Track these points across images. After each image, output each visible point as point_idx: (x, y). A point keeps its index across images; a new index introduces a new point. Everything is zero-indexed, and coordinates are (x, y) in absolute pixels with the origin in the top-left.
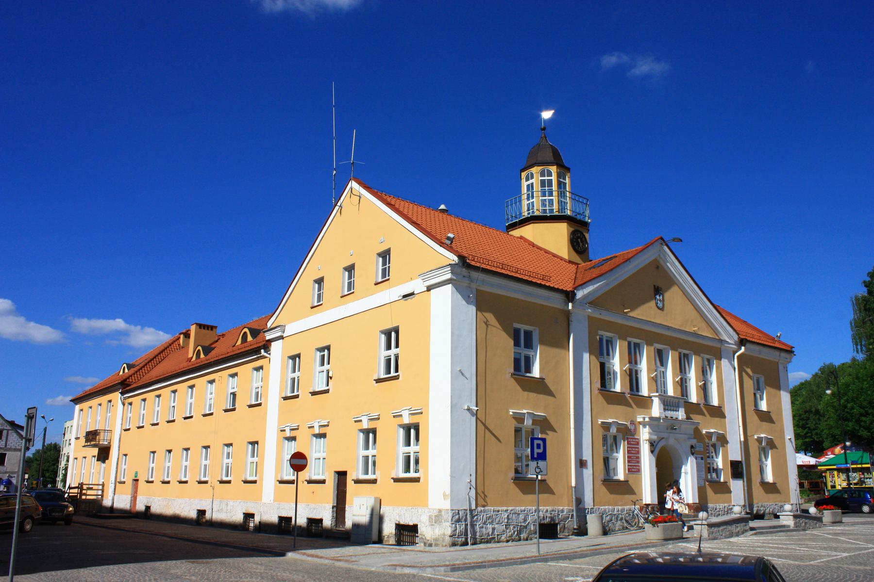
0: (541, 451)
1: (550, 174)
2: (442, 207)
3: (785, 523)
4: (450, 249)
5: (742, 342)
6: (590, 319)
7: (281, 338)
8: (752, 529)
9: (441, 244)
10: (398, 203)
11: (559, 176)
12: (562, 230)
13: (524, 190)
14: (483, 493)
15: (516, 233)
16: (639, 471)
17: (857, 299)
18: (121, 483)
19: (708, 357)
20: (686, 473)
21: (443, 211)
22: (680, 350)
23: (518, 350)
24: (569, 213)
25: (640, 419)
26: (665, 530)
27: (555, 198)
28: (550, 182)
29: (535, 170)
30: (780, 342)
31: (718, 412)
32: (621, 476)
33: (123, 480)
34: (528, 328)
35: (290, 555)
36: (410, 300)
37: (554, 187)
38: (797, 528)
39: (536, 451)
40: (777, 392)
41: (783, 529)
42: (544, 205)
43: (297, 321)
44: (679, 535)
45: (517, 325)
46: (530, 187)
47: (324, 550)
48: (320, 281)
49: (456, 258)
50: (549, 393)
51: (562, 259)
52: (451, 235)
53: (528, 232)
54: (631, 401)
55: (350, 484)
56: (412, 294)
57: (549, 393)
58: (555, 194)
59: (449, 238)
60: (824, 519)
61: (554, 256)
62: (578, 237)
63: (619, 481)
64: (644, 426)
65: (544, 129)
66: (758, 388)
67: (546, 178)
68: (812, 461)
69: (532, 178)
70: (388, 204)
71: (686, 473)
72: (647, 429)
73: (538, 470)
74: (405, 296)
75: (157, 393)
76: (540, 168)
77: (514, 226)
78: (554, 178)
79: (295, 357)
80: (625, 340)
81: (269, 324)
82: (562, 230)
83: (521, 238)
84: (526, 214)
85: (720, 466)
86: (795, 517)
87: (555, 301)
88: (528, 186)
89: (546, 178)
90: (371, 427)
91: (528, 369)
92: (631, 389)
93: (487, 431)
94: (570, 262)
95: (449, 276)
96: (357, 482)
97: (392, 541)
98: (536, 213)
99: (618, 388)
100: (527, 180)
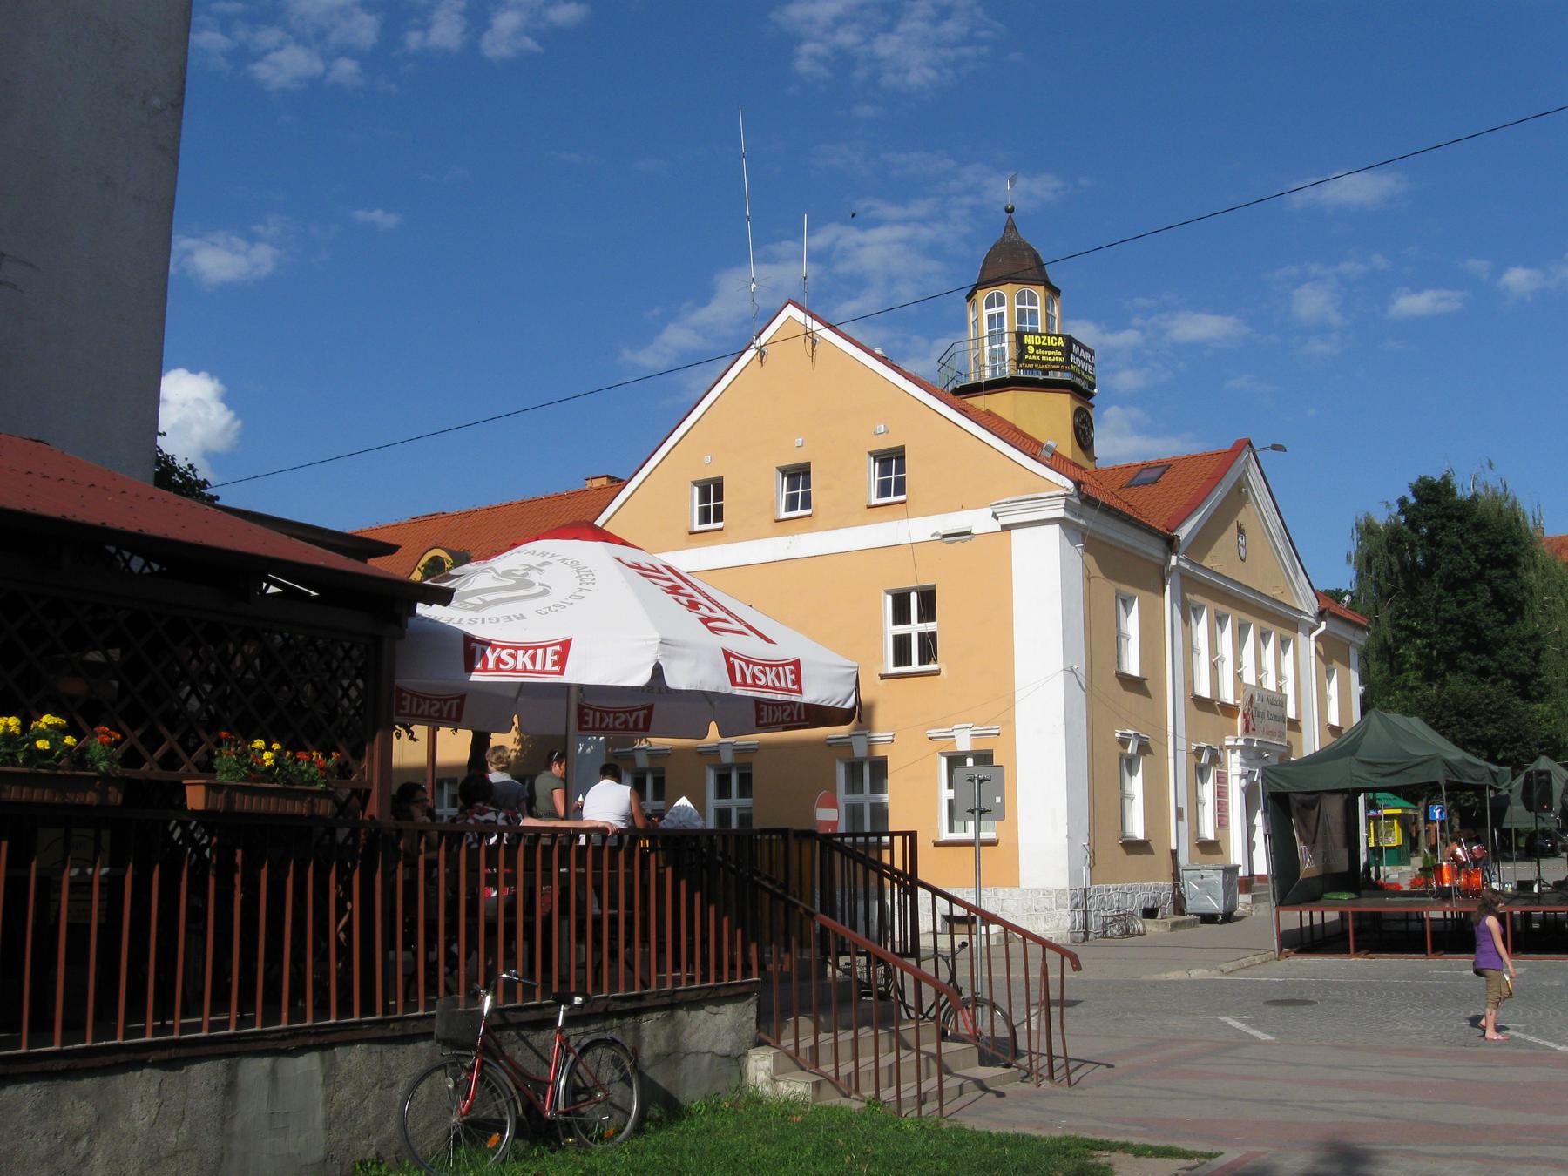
1: (1033, 301)
5: (1321, 615)
11: (1048, 305)
12: (1062, 405)
16: (1227, 824)
17: (1367, 530)
19: (739, 691)
25: (1227, 743)
29: (1007, 290)
36: (958, 546)
49: (1070, 485)
50: (1146, 693)
51: (1065, 459)
56: (969, 533)
57: (1146, 693)
64: (1233, 751)
69: (1001, 303)
74: (945, 536)
76: (1017, 288)
84: (988, 375)
87: (1154, 549)
100: (989, 305)
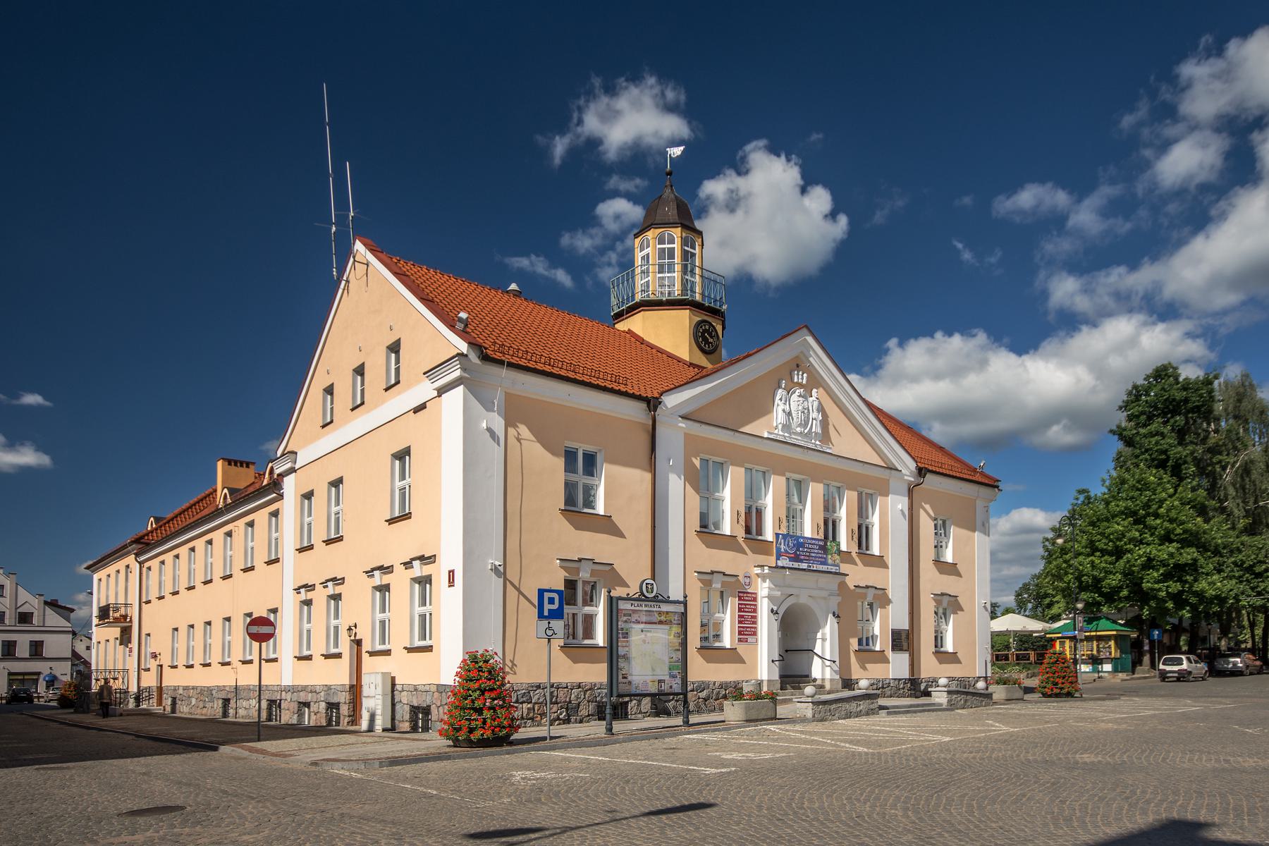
0: (555, 606)
2: (513, 286)
3: (937, 700)
4: (463, 334)
6: (687, 436)
7: (292, 470)
8: (882, 708)
9: (452, 327)
10: (407, 267)
11: (685, 242)
12: (683, 320)
13: (638, 262)
14: (512, 662)
15: (622, 326)
18: (267, 661)
20: (824, 640)
21: (517, 294)
22: (788, 475)
23: (573, 477)
24: (698, 297)
26: (747, 708)
27: (677, 275)
28: (672, 251)
29: (651, 234)
30: (982, 474)
31: (880, 562)
32: (727, 642)
33: (272, 656)
34: (590, 448)
35: (225, 749)
37: (677, 259)
38: (952, 706)
39: (547, 607)
40: (970, 533)
41: (936, 708)
42: (662, 286)
43: (311, 445)
44: (770, 714)
45: (572, 444)
46: (646, 258)
47: (274, 742)
48: (329, 390)
51: (679, 360)
52: (463, 315)
53: (637, 324)
54: (857, 560)
55: (365, 656)
58: (678, 268)
59: (460, 320)
60: (995, 697)
61: (670, 356)
62: (705, 331)
63: (947, 653)
65: (670, 174)
66: (941, 528)
67: (666, 246)
68: (1035, 626)
70: (399, 275)
71: (824, 640)
72: (767, 584)
73: (550, 633)
75: (190, 545)
77: (619, 316)
78: (677, 246)
79: (308, 496)
80: (783, 475)
81: (279, 453)
82: (683, 320)
83: (630, 332)
84: (638, 297)
85: (877, 631)
86: (949, 692)
88: (643, 258)
89: (666, 246)
90: (384, 583)
91: (589, 503)
92: (748, 531)
93: (517, 584)
94: (691, 365)
95: (457, 373)
96: (372, 654)
97: (406, 726)
98: (652, 297)
99: (726, 529)
